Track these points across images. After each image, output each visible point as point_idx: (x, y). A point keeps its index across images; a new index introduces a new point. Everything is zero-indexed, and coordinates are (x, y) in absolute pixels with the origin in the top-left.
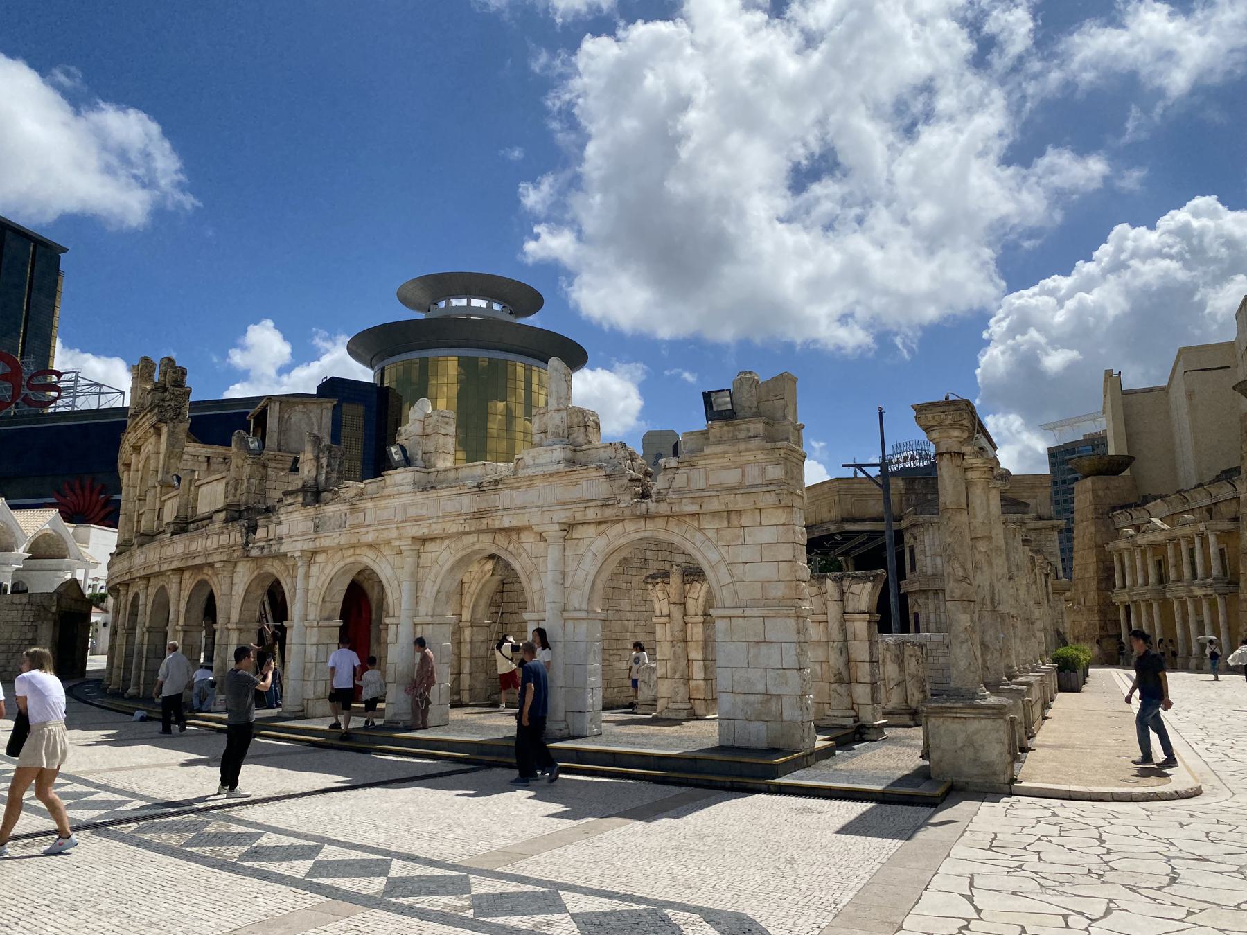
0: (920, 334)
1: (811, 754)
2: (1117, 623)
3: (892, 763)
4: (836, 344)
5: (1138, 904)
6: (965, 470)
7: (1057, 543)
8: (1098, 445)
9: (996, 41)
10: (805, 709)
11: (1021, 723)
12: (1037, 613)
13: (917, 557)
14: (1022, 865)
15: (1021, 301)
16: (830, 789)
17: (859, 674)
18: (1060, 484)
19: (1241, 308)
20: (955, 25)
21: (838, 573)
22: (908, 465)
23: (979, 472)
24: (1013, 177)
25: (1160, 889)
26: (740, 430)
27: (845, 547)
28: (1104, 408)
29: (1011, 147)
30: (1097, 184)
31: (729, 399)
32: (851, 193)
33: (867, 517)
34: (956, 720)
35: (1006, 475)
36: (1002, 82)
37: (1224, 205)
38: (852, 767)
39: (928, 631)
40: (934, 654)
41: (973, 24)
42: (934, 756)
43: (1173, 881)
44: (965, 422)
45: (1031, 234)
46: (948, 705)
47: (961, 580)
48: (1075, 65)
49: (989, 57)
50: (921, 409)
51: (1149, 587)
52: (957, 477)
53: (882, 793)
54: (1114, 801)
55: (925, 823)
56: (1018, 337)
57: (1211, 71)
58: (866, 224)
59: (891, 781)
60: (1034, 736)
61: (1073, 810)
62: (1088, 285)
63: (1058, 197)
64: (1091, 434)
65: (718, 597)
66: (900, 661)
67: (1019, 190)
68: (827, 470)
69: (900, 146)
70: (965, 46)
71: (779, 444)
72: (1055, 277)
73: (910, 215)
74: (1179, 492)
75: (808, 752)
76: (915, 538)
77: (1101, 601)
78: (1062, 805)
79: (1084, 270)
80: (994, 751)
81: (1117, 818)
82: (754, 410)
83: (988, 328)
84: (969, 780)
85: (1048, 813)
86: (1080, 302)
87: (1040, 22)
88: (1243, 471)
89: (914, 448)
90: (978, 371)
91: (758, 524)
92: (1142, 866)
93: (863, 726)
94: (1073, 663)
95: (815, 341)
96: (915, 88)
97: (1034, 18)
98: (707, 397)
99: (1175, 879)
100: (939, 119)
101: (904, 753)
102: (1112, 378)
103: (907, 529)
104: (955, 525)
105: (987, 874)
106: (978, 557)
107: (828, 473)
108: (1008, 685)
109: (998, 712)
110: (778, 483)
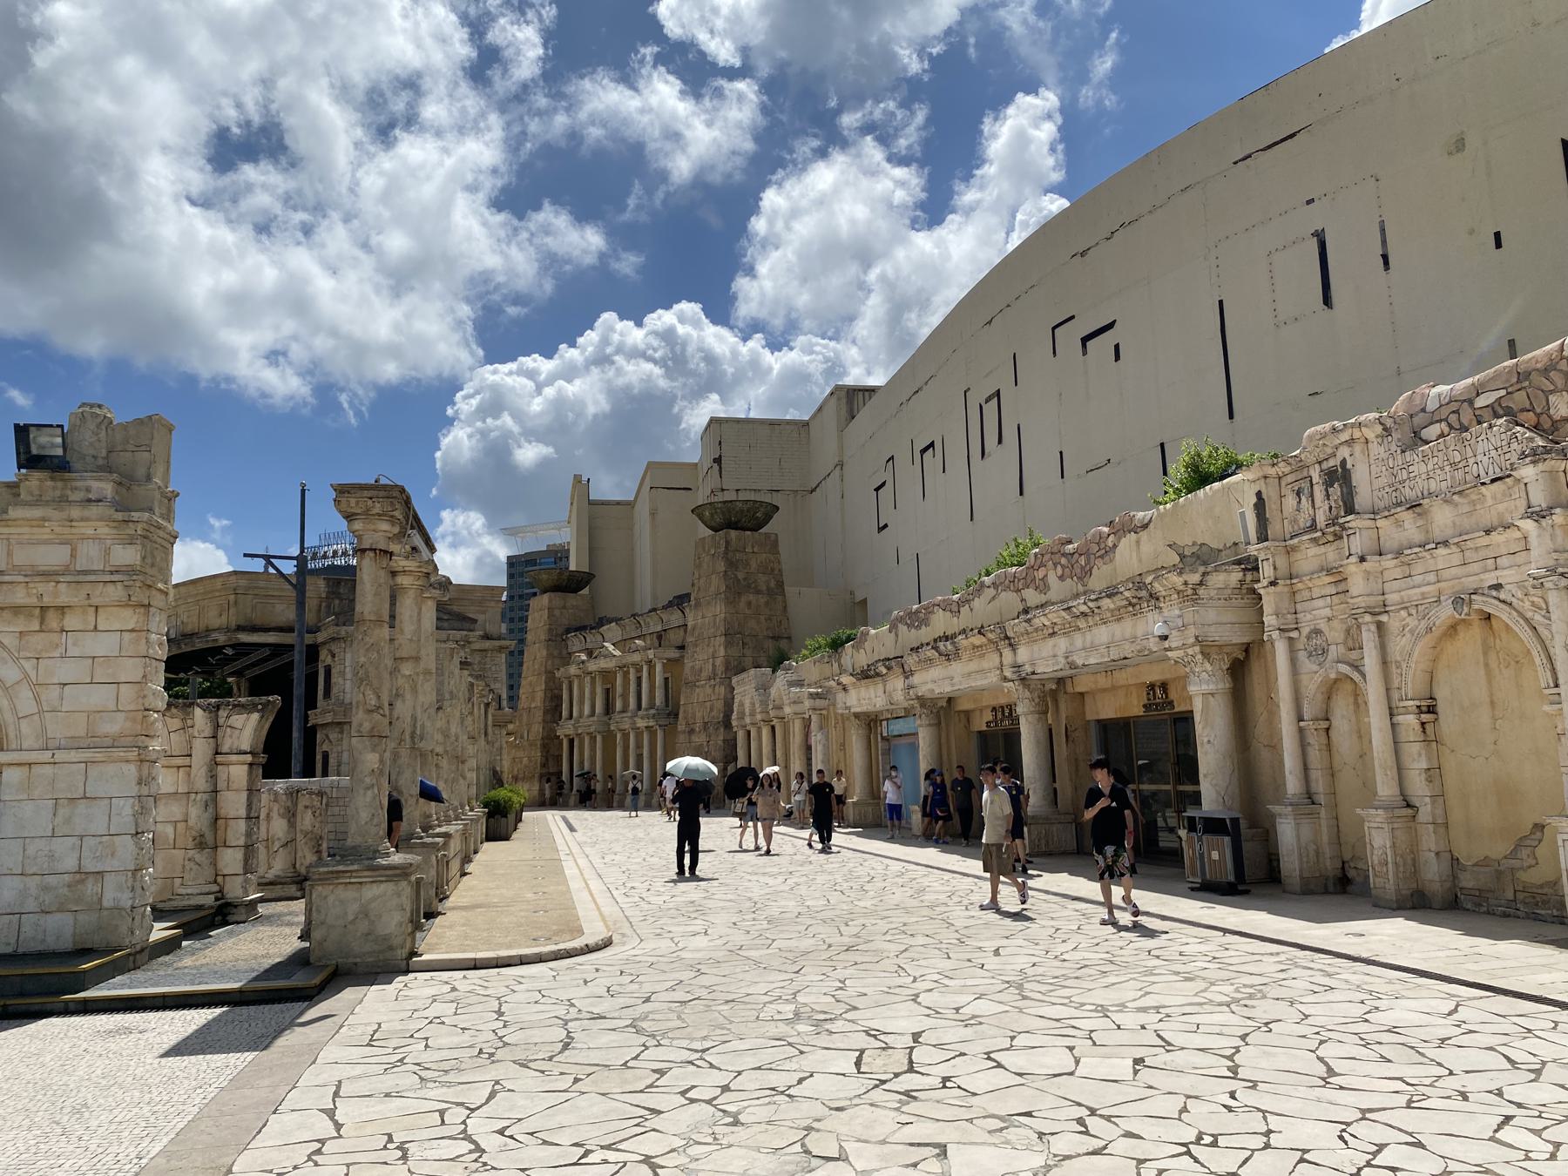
0: (372, 394)
1: (142, 950)
2: (559, 758)
3: (260, 950)
4: (259, 389)
5: (526, 1080)
6: (394, 574)
7: (504, 667)
8: (561, 559)
9: (500, 56)
10: (139, 891)
11: (432, 883)
12: (471, 750)
13: (333, 681)
14: (404, 1058)
15: (496, 378)
16: (164, 996)
17: (230, 834)
18: (516, 598)
19: (706, 429)
20: (453, 18)
21: (214, 700)
22: (337, 562)
23: (412, 578)
24: (504, 225)
25: (550, 1059)
26: (74, 489)
27: (238, 665)
28: (570, 517)
29: (504, 190)
30: (590, 260)
31: (59, 440)
32: (299, 192)
33: (273, 625)
34: (350, 886)
35: (446, 583)
36: (502, 107)
37: (707, 317)
38: (204, 961)
39: (339, 775)
40: (341, 804)
41: (477, 27)
42: (316, 935)
43: (566, 1046)
44: (397, 514)
45: (518, 299)
46: (341, 868)
47: (372, 711)
48: (583, 115)
49: (489, 72)
50: (342, 490)
52: (382, 581)
53: (240, 991)
54: (522, 964)
55: (292, 1024)
56: (489, 420)
57: (713, 167)
58: (316, 238)
59: (254, 974)
60: (447, 897)
61: (475, 981)
62: (569, 374)
63: (550, 262)
64: (555, 545)
65: (12, 735)
66: (291, 815)
67: (509, 244)
68: (229, 559)
69: (372, 149)
70: (463, 50)
71: (135, 515)
72: (536, 356)
73: (375, 240)
74: (634, 616)
75: (138, 948)
76: (333, 656)
77: (545, 734)
78: (465, 977)
79: (567, 355)
80: (393, 922)
81: (521, 983)
82: (100, 462)
83: (454, 404)
84: (358, 960)
85: (447, 988)
86: (560, 390)
87: (550, 52)
88: (692, 598)
89: (348, 542)
90: (438, 454)
91: (92, 628)
92: (537, 1035)
93: (228, 905)
94: (505, 807)
95: (229, 379)
96: (397, 78)
97: (545, 46)
98: (22, 432)
99: (569, 1044)
100: (423, 129)
101: (281, 934)
102: (580, 484)
103: (324, 643)
104: (372, 641)
105: (360, 1077)
106: (401, 681)
107: (230, 563)
108: (421, 838)
109: (402, 872)
110: (130, 571)
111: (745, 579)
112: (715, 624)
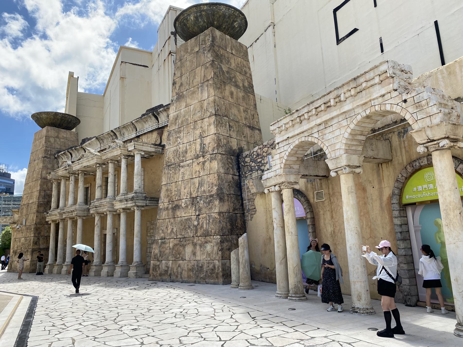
51: (77, 206)
77: (38, 220)
111: (228, 72)
112: (202, 107)
